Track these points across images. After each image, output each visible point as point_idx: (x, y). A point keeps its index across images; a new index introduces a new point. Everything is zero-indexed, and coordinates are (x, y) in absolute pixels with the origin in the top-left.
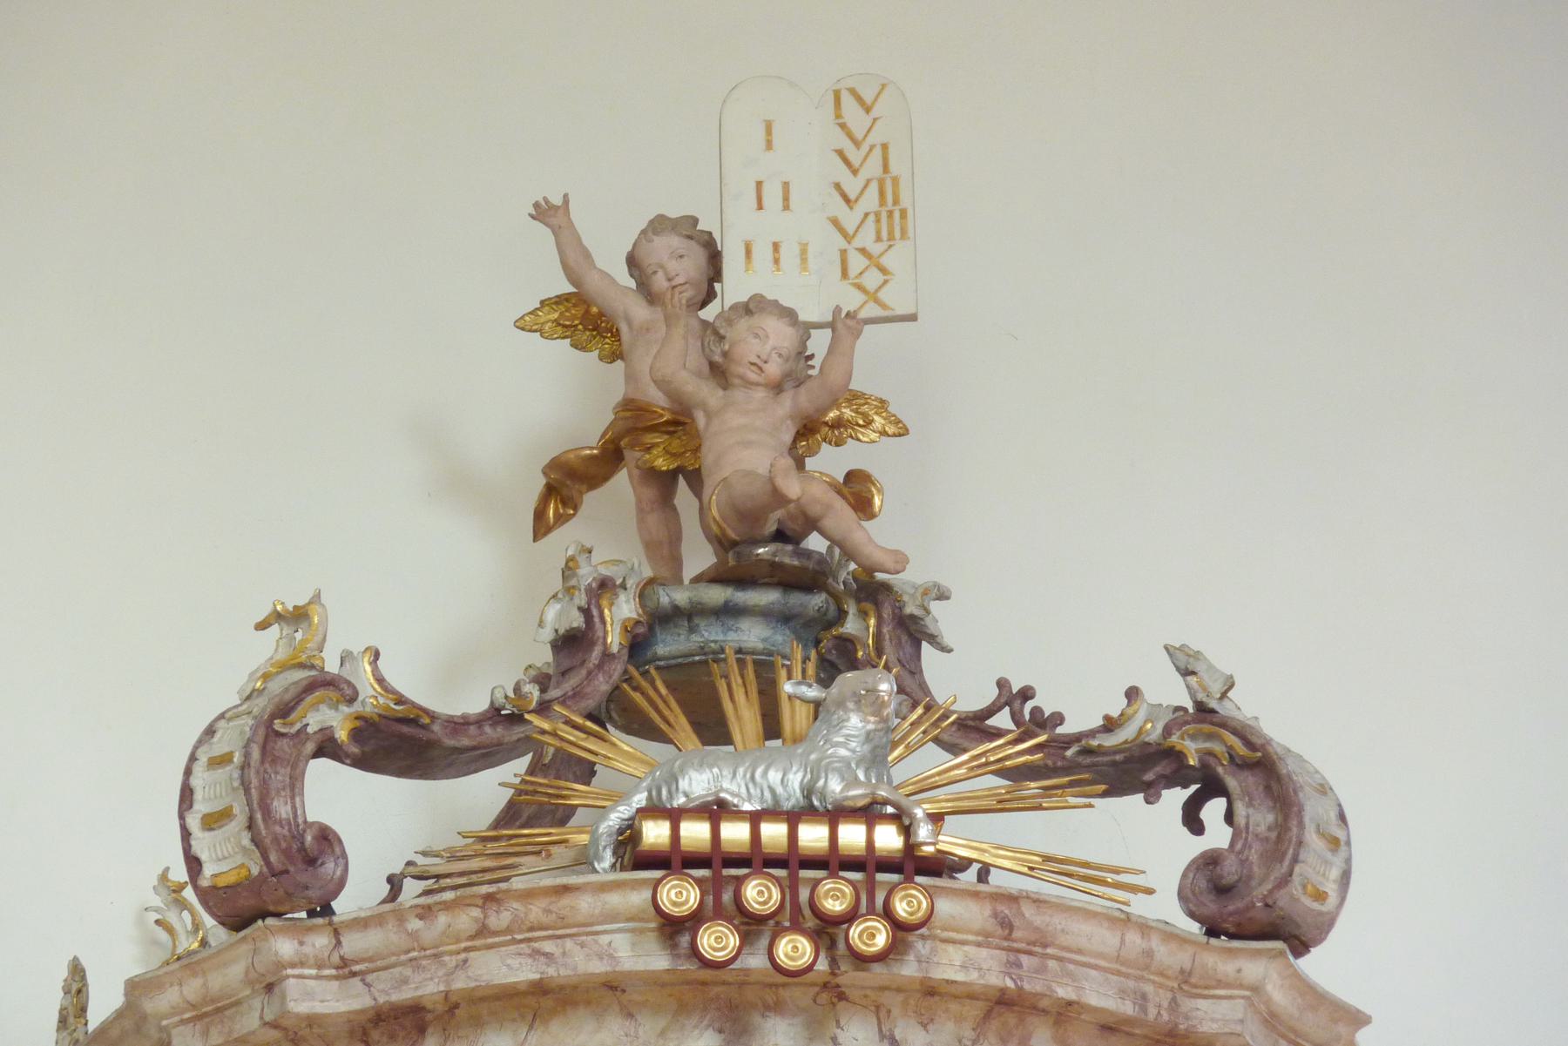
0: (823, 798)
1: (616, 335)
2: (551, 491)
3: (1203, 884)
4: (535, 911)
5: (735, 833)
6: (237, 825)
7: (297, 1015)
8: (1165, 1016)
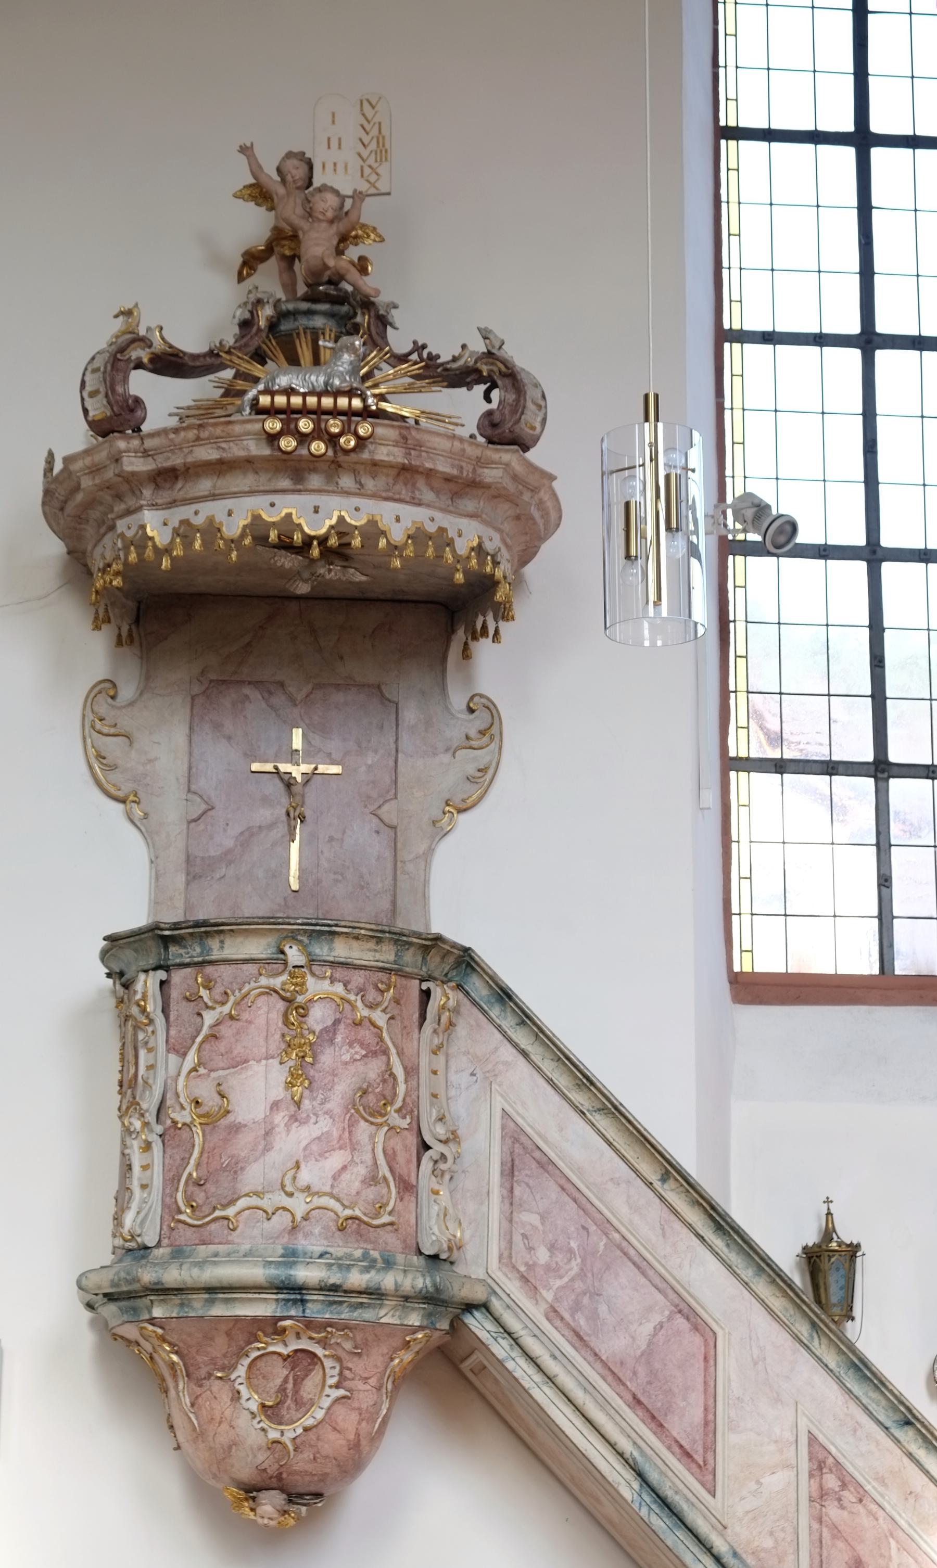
0: (332, 387)
1: (272, 200)
2: (245, 264)
3: (487, 423)
4: (218, 431)
5: (296, 401)
6: (101, 396)
7: (128, 472)
8: (470, 475)
